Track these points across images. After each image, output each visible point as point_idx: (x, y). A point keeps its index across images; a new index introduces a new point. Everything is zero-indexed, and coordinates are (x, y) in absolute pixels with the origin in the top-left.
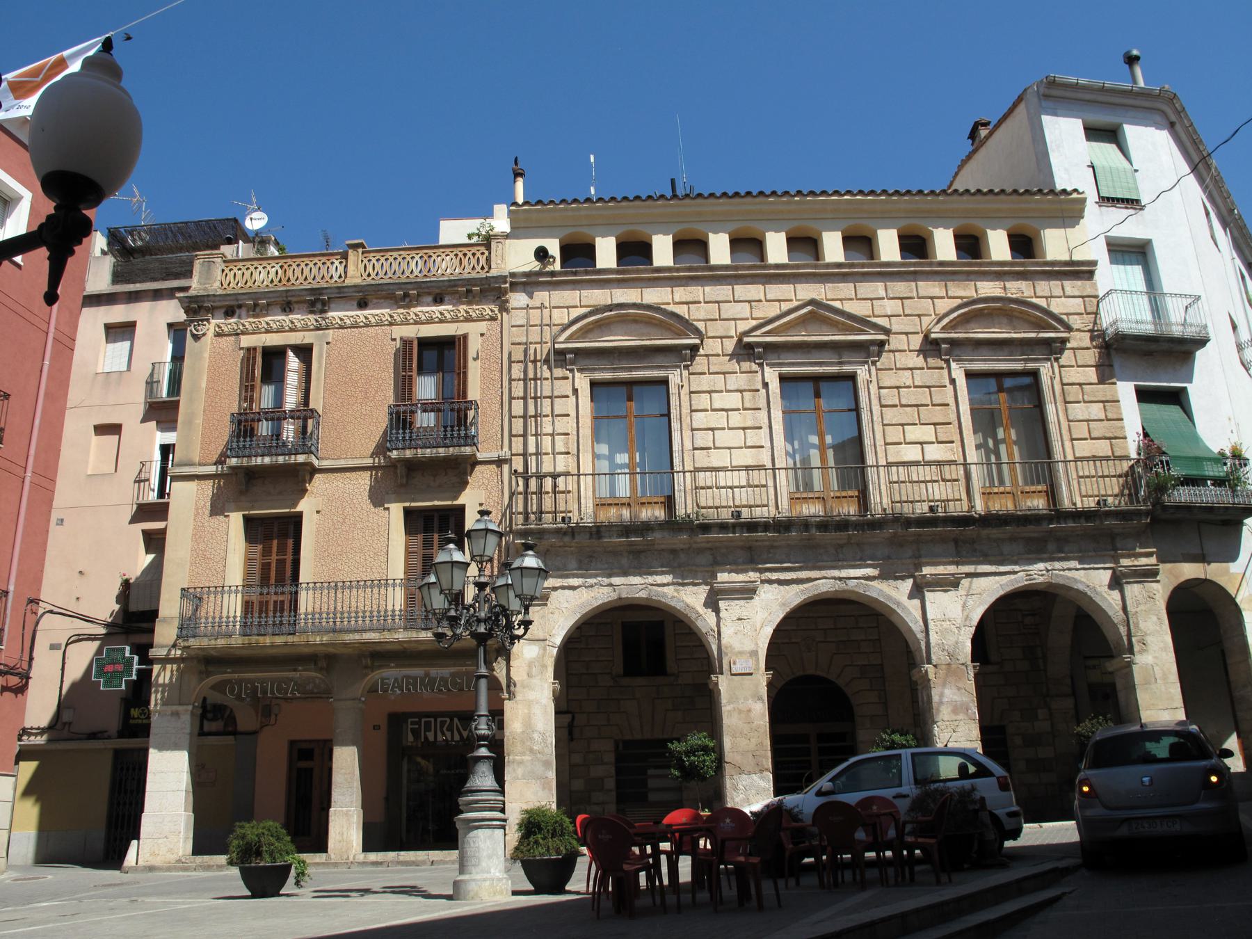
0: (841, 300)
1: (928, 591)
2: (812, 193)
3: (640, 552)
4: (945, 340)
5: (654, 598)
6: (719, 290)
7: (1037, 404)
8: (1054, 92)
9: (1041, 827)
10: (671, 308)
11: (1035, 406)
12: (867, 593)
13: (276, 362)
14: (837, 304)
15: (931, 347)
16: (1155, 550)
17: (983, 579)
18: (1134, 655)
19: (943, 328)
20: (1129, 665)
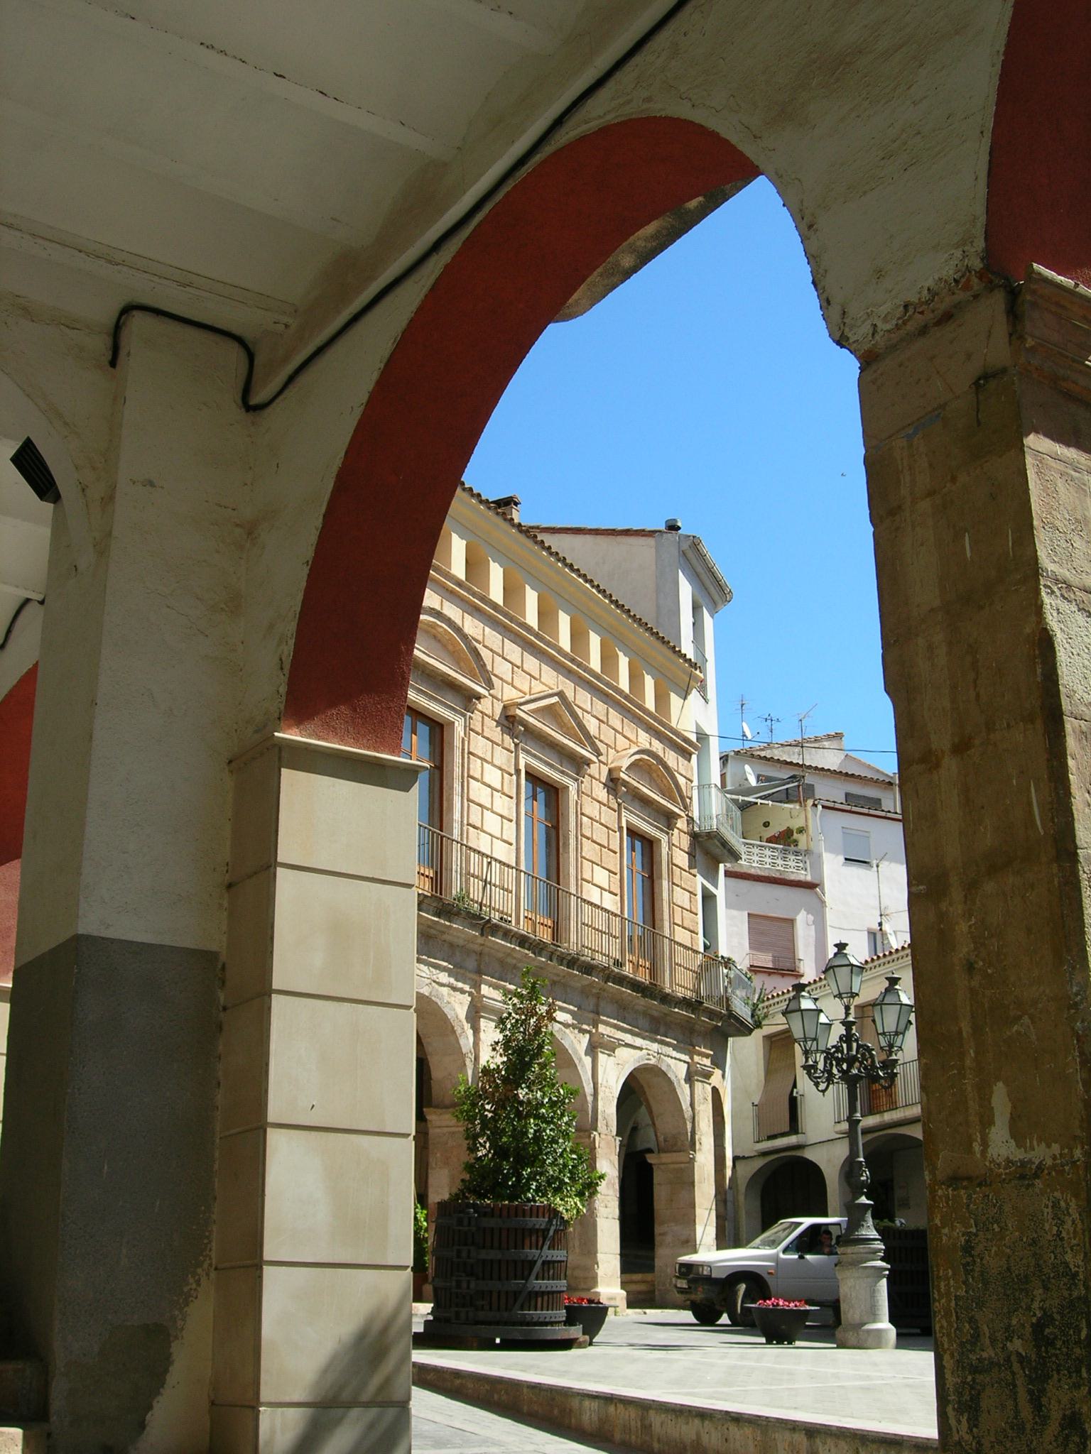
0: (583, 710)
1: (601, 1052)
2: (571, 566)
3: (431, 937)
4: (625, 784)
5: (433, 998)
6: (494, 636)
7: (555, 824)
8: (690, 554)
9: (645, 1313)
10: (479, 647)
11: (436, 767)
12: (562, 1041)
13: (663, 819)
14: (579, 712)
15: (509, 722)
16: (712, 1053)
17: (282, 996)
18: (695, 1152)
19: (534, 711)
20: (692, 1161)
